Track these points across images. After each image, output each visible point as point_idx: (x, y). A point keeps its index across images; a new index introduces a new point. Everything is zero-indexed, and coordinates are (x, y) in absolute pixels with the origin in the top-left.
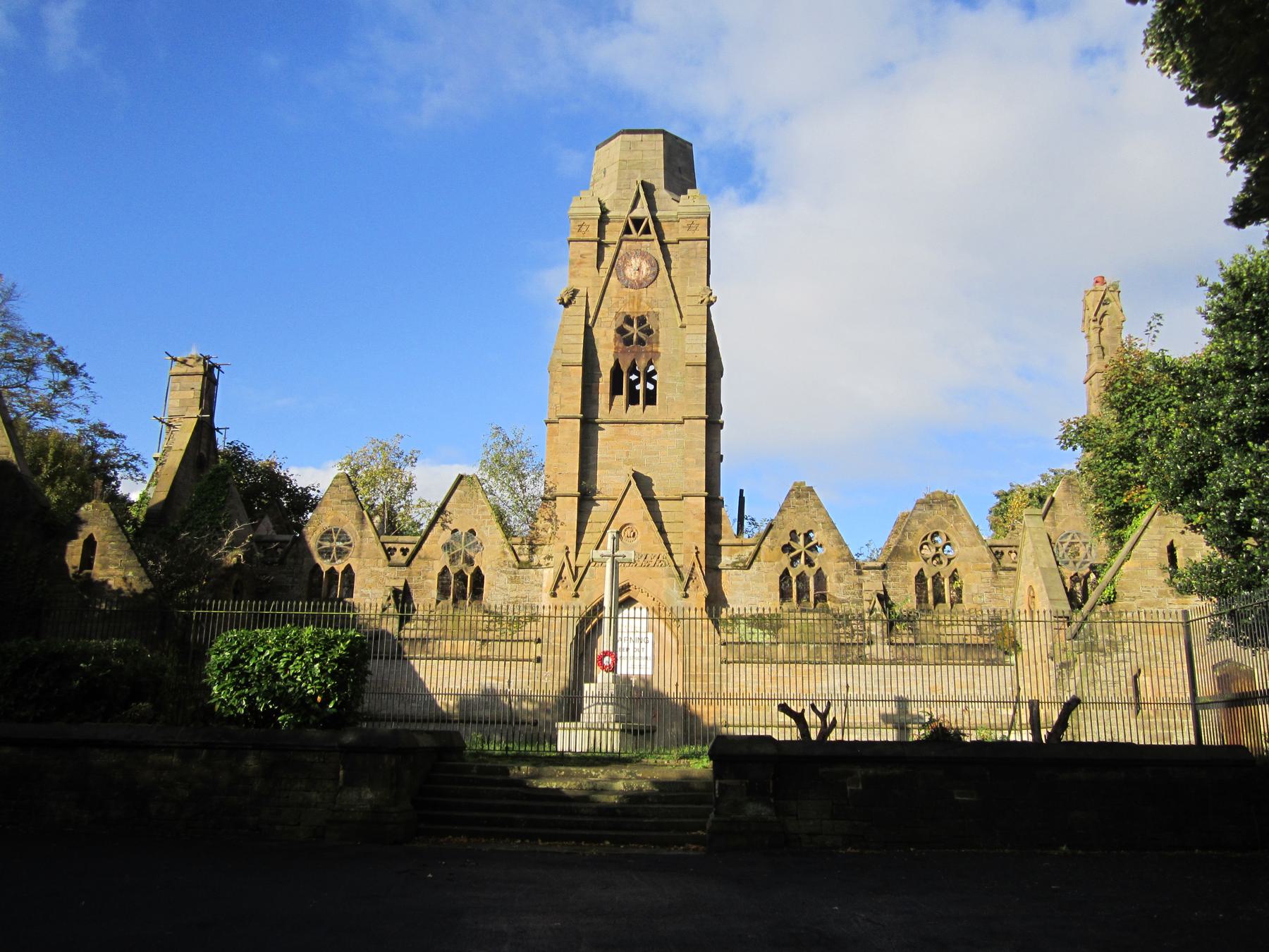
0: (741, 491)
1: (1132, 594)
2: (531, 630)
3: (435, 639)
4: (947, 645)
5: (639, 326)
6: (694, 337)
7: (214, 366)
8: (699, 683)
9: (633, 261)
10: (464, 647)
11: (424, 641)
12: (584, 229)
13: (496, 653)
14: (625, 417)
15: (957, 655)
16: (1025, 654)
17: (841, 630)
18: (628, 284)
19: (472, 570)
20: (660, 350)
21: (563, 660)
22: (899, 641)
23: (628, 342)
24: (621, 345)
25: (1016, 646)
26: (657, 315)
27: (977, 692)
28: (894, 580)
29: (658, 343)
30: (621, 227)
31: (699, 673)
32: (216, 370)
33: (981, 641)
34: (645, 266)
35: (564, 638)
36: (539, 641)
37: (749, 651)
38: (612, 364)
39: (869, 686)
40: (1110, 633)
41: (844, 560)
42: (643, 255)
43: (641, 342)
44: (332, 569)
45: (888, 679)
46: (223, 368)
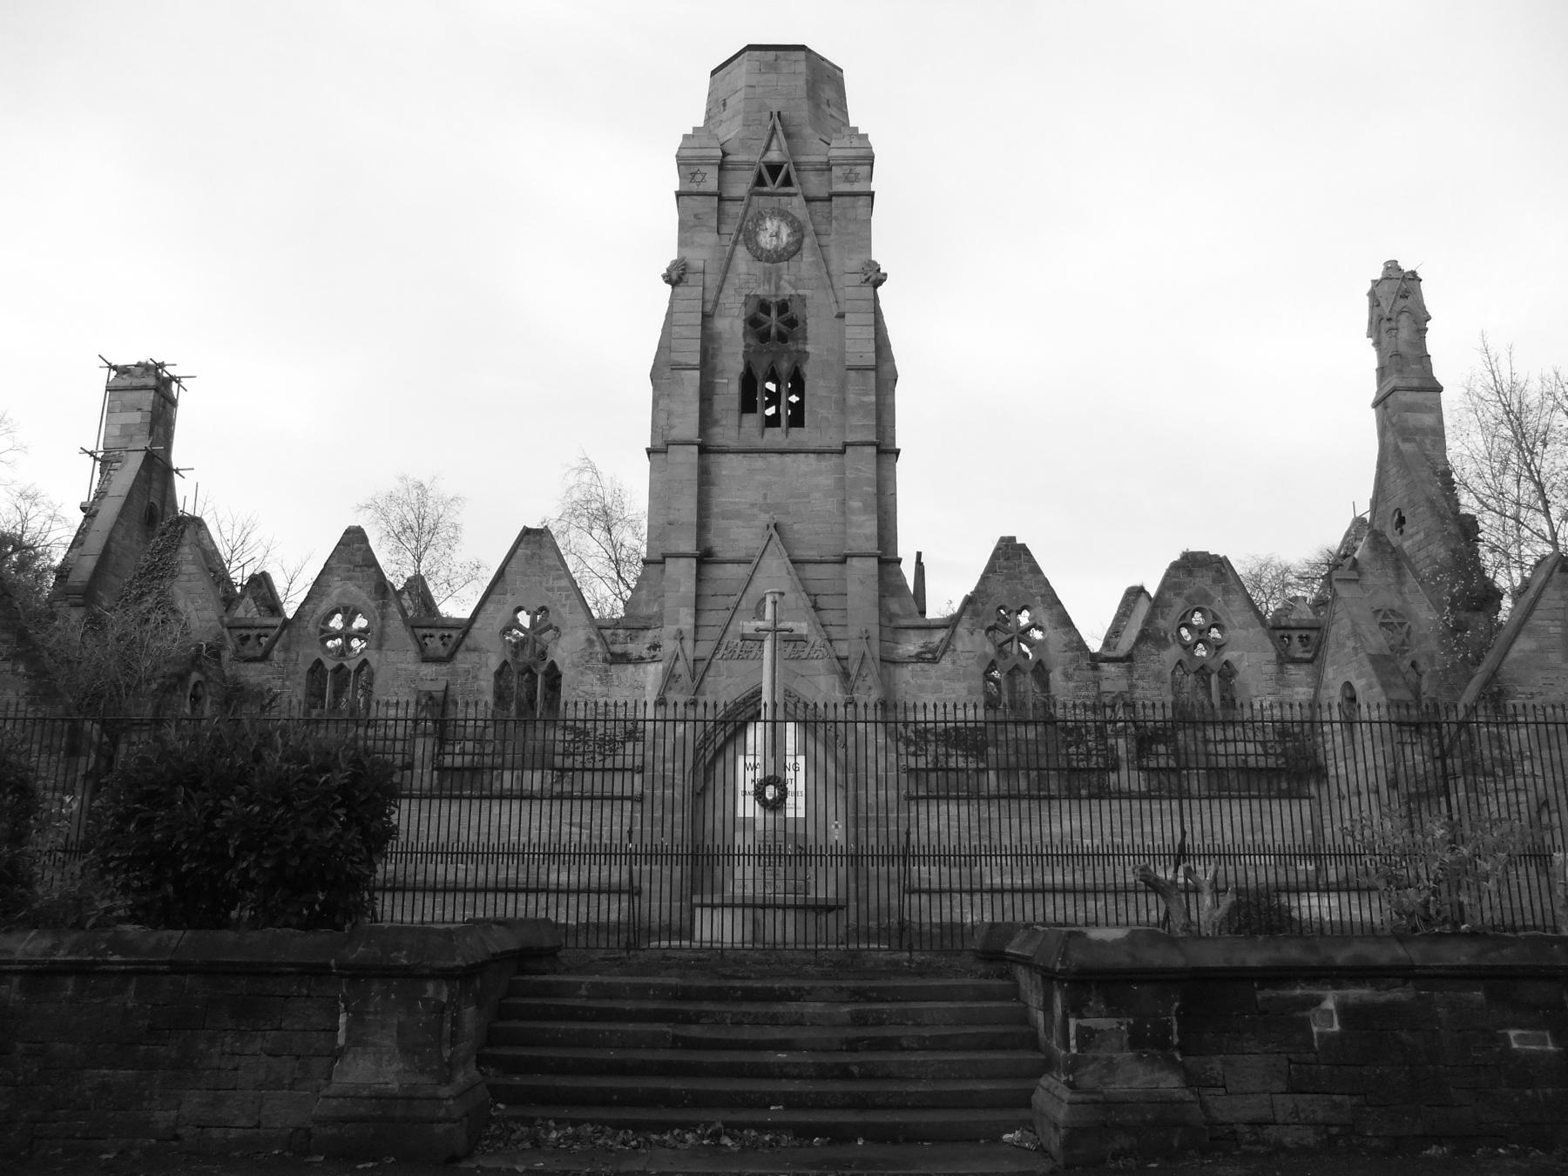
0: (919, 555)
1: (1527, 690)
2: (630, 753)
3: (493, 768)
4: (1218, 770)
5: (780, 313)
6: (857, 330)
7: (172, 378)
8: (872, 829)
9: (768, 224)
10: (534, 780)
11: (475, 770)
12: (698, 178)
13: (577, 788)
14: (761, 443)
15: (1235, 785)
16: (1333, 781)
17: (1072, 750)
18: (759, 254)
19: (543, 668)
20: (809, 348)
21: (678, 796)
22: (1153, 764)
23: (764, 337)
24: (753, 342)
25: (1320, 773)
26: (803, 299)
27: (1268, 838)
28: (1142, 678)
29: (805, 339)
30: (750, 176)
31: (872, 814)
32: (174, 386)
33: (1271, 762)
34: (785, 232)
35: (679, 764)
36: (642, 770)
37: (942, 782)
38: (741, 368)
39: (1117, 830)
40: (1501, 748)
41: (1072, 649)
42: (784, 215)
43: (782, 338)
44: (341, 666)
45: (1137, 819)
46: (184, 382)
